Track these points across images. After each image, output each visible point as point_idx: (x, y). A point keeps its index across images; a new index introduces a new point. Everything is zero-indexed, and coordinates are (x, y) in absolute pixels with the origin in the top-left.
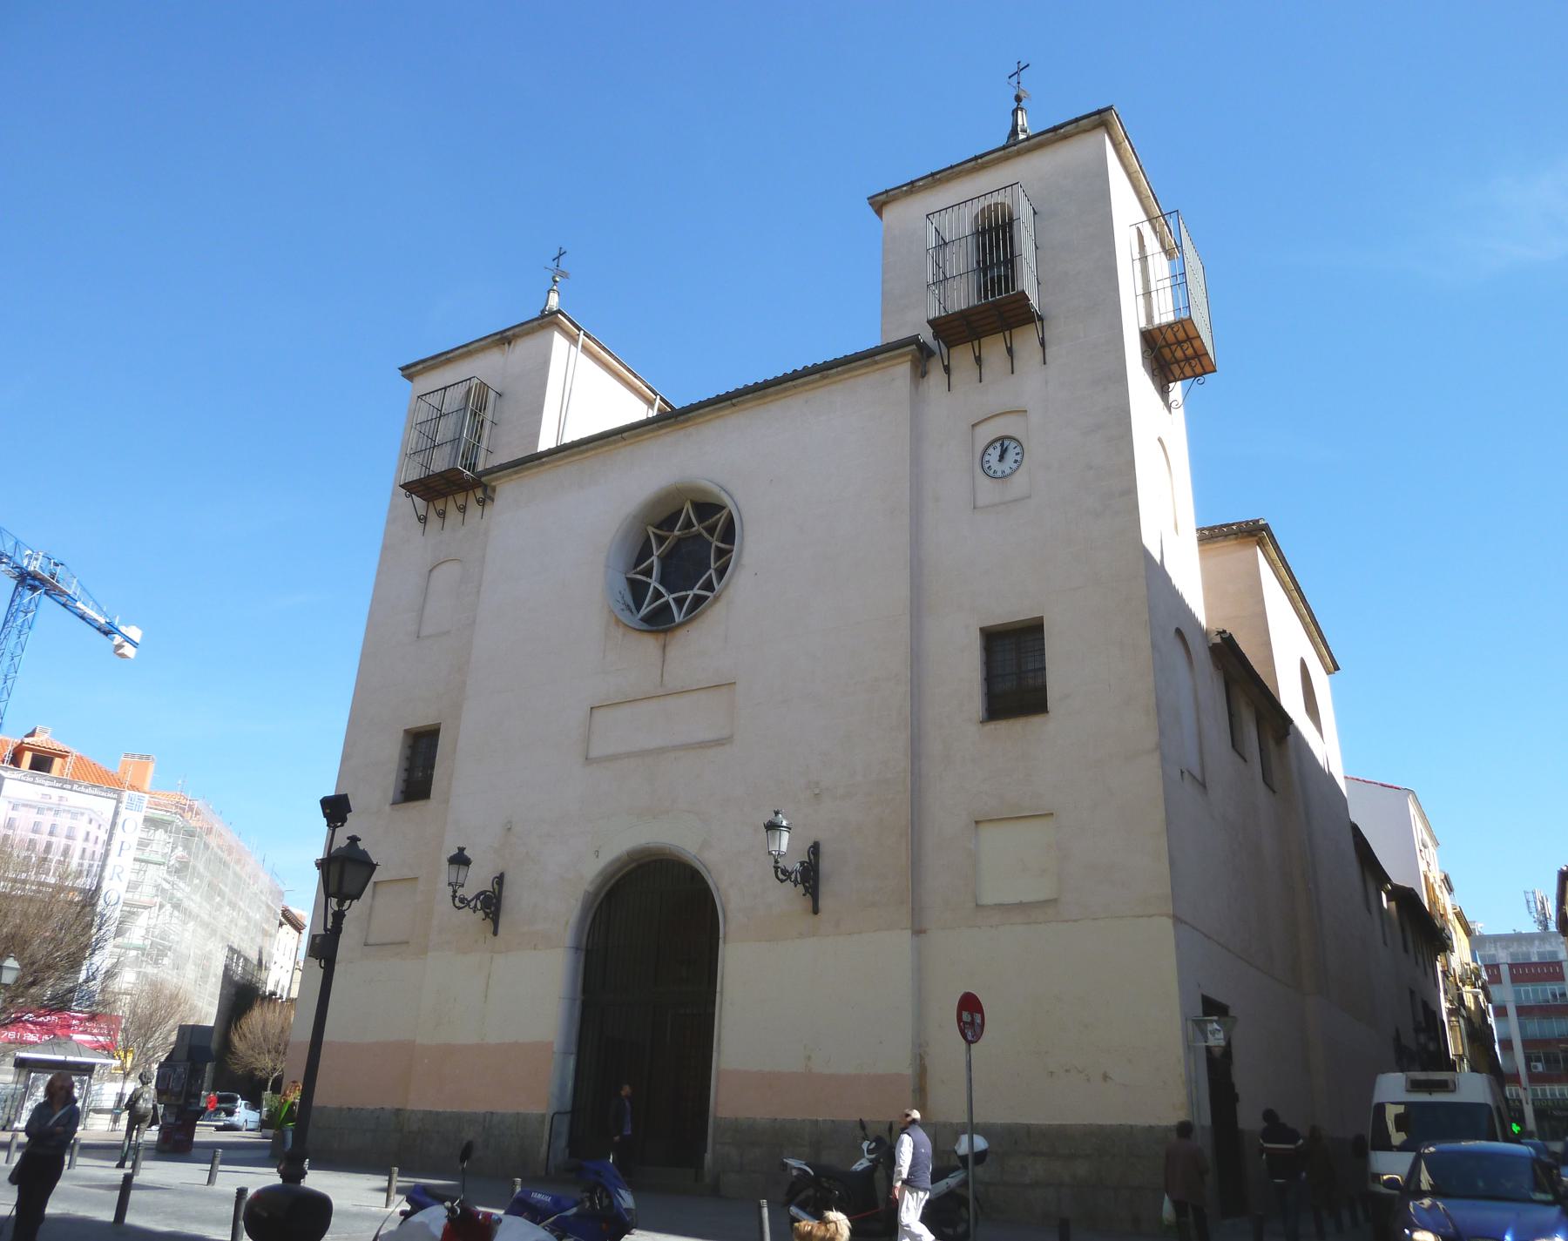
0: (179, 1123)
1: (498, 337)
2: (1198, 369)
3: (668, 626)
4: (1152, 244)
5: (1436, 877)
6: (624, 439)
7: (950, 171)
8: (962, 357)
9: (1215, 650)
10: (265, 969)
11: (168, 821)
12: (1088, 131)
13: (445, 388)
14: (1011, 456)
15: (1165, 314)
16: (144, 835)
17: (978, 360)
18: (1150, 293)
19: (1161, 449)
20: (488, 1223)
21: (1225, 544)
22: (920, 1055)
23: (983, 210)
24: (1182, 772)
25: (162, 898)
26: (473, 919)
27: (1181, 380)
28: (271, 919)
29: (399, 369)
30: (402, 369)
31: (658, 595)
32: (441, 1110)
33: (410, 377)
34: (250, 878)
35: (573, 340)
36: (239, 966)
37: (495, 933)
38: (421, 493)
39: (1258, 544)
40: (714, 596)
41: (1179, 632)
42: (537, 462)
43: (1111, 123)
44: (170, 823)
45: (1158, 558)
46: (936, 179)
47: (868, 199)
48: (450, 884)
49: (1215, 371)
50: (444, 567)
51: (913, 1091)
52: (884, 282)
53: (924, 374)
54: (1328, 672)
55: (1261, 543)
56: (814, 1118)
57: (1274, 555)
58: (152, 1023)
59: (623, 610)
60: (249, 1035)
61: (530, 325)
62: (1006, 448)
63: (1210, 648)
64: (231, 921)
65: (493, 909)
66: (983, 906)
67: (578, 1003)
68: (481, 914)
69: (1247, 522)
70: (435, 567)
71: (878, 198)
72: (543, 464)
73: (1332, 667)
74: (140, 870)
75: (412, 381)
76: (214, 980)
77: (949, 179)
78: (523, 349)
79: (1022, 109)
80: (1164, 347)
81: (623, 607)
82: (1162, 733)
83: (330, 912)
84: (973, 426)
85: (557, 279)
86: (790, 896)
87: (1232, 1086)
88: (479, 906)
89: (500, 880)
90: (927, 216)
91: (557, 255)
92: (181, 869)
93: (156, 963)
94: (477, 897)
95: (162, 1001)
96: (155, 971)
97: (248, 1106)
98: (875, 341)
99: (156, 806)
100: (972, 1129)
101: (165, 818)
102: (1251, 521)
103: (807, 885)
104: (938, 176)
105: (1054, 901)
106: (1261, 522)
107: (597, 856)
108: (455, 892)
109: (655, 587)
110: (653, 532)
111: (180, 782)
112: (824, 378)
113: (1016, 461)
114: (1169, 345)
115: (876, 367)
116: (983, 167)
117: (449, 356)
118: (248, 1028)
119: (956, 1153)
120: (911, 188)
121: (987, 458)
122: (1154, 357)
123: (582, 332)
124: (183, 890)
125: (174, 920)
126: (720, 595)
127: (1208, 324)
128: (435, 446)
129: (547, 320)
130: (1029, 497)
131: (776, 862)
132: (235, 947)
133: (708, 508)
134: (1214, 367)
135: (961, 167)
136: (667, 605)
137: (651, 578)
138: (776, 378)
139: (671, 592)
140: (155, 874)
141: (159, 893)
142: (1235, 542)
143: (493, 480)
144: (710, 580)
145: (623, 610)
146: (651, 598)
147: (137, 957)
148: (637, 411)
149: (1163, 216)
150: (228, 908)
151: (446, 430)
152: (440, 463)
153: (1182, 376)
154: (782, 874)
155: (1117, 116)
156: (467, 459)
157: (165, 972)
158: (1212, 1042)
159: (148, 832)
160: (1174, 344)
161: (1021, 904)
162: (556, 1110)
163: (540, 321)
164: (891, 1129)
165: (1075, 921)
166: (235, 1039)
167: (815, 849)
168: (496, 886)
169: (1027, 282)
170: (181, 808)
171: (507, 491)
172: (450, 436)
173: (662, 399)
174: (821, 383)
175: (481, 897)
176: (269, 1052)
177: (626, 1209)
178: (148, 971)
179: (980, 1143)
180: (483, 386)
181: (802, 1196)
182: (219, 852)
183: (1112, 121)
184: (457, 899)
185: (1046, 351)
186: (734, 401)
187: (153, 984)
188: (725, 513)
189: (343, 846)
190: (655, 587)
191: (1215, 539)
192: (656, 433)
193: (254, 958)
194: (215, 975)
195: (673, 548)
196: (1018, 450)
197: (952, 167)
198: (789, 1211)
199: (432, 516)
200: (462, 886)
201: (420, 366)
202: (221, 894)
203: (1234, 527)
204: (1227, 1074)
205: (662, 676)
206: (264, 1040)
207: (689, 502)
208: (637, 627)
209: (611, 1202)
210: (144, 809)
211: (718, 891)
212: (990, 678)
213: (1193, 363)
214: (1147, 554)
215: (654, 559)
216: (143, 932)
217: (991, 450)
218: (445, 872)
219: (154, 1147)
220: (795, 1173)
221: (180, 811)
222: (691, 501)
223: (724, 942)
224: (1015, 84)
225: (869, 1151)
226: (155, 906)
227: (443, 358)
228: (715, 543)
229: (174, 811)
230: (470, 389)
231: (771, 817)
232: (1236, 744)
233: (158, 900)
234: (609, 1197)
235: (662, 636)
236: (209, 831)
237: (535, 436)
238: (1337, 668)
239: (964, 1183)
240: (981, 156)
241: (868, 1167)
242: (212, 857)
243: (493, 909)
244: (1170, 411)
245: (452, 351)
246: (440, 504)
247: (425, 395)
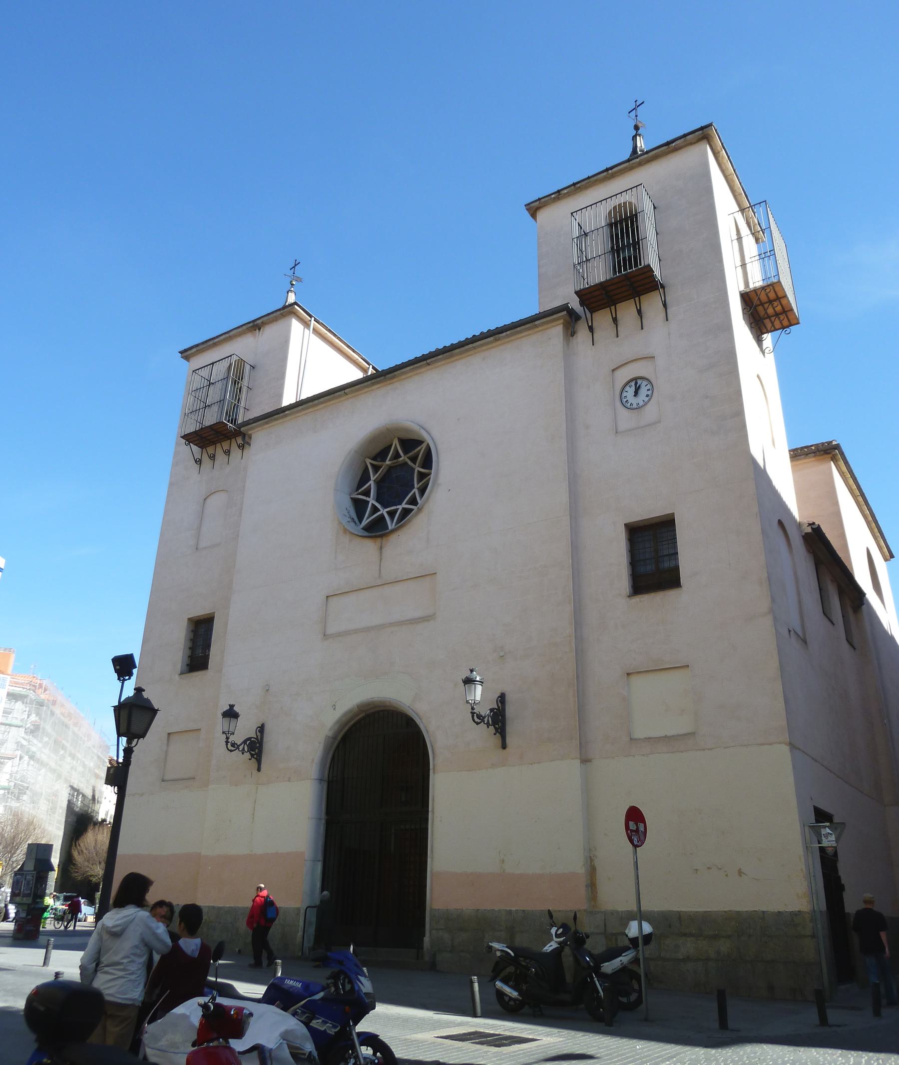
0: (30, 917)
2: (785, 323)
3: (383, 532)
6: (346, 394)
7: (588, 181)
8: (602, 319)
9: (807, 538)
10: (98, 803)
11: (24, 695)
12: (695, 143)
13: (213, 364)
14: (643, 391)
15: (756, 280)
16: (7, 706)
17: (615, 320)
20: (239, 1017)
21: (806, 461)
22: (590, 857)
23: (615, 208)
24: (789, 631)
25: (21, 751)
26: (242, 758)
27: (771, 331)
28: (101, 766)
29: (179, 352)
30: (181, 352)
32: (221, 905)
34: (85, 736)
35: (306, 325)
36: (78, 800)
37: (259, 770)
38: (198, 442)
39: (832, 460)
40: (418, 508)
41: (780, 523)
42: (282, 414)
43: (711, 136)
44: (26, 696)
45: (761, 464)
46: (577, 187)
48: (223, 733)
49: (798, 323)
50: (213, 497)
51: (586, 886)
52: (539, 267)
53: (573, 334)
54: (886, 560)
55: (834, 459)
56: (508, 909)
57: (844, 468)
58: (15, 844)
59: (349, 522)
60: (85, 851)
61: (275, 314)
62: (640, 386)
63: (803, 537)
64: (72, 768)
65: (257, 750)
66: (636, 739)
67: (323, 821)
68: (247, 755)
70: (207, 497)
72: (286, 416)
73: (889, 555)
74: (5, 732)
75: (189, 362)
76: (61, 811)
77: (586, 187)
78: (270, 332)
79: (640, 135)
81: (349, 520)
82: (773, 600)
83: (121, 748)
84: (613, 370)
85: (294, 283)
86: (484, 734)
88: (246, 749)
89: (261, 729)
90: (572, 214)
91: (296, 267)
92: (34, 730)
93: (18, 799)
94: (245, 742)
95: (21, 827)
96: (18, 805)
97: (86, 903)
98: (533, 310)
99: (16, 684)
100: (641, 916)
101: (22, 693)
102: (826, 443)
103: (497, 726)
104: (579, 185)
105: (692, 734)
106: (834, 443)
107: (335, 709)
108: (227, 738)
109: (372, 504)
110: (370, 463)
111: (32, 666)
112: (496, 340)
113: (647, 396)
114: (762, 304)
115: (536, 330)
116: (613, 176)
118: (84, 845)
119: (627, 936)
120: (559, 195)
121: (625, 394)
122: (751, 313)
123: (313, 319)
124: (36, 746)
125: (30, 768)
126: (422, 508)
127: (792, 287)
128: (206, 406)
129: (287, 311)
130: (659, 422)
131: (473, 709)
132: (75, 786)
133: (411, 443)
134: (798, 320)
135: (595, 178)
136: (382, 517)
137: (369, 497)
138: (460, 342)
139: (385, 507)
140: (17, 734)
141: (19, 748)
142: (814, 459)
144: (414, 497)
145: (349, 522)
146: (369, 515)
147: (4, 794)
148: (356, 375)
149: (751, 206)
150: (69, 758)
151: (214, 394)
152: (210, 419)
153: (773, 328)
154: (477, 718)
155: (716, 131)
156: (230, 416)
157: (25, 806)
158: (825, 843)
159: (10, 703)
160: (766, 303)
161: (666, 736)
162: (308, 905)
164: (575, 918)
165: (711, 749)
166: (75, 854)
167: (502, 698)
168: (259, 734)
169: (651, 257)
170: (33, 686)
171: (260, 437)
172: (217, 399)
173: (373, 368)
174: (494, 344)
175: (248, 742)
176: (100, 863)
177: (364, 993)
178: (12, 805)
179: (647, 928)
180: (241, 362)
181: (502, 975)
182: (62, 718)
183: (713, 135)
184: (229, 744)
185: (668, 311)
186: (428, 361)
187: (15, 815)
188: (424, 446)
190: (372, 504)
191: (798, 457)
192: (370, 389)
193: (89, 794)
194: (61, 807)
195: (385, 475)
196: (649, 387)
197: (589, 178)
198: (495, 985)
199: (205, 458)
200: (233, 734)
201: (194, 350)
202: (64, 748)
203: (813, 448)
204: (835, 869)
205: (380, 570)
206: (96, 855)
208: (360, 534)
209: (353, 988)
210: (7, 687)
211: (428, 733)
212: (634, 563)
214: (754, 462)
215: (371, 483)
216: (8, 777)
217: (627, 388)
218: (220, 724)
219: (11, 935)
220: (498, 954)
221: (34, 688)
222: (398, 438)
223: (434, 773)
224: (634, 117)
225: (557, 936)
226: (16, 757)
227: (211, 343)
228: (418, 469)
229: (28, 688)
230: (231, 365)
231: (468, 674)
232: (826, 613)
233: (19, 753)
234: (350, 982)
235: (379, 540)
236: (54, 703)
237: (280, 396)
238: (892, 556)
239: (636, 961)
241: (557, 947)
242: (57, 721)
243: (257, 750)
244: (764, 355)
245: (217, 337)
246: (211, 450)
247: (198, 369)
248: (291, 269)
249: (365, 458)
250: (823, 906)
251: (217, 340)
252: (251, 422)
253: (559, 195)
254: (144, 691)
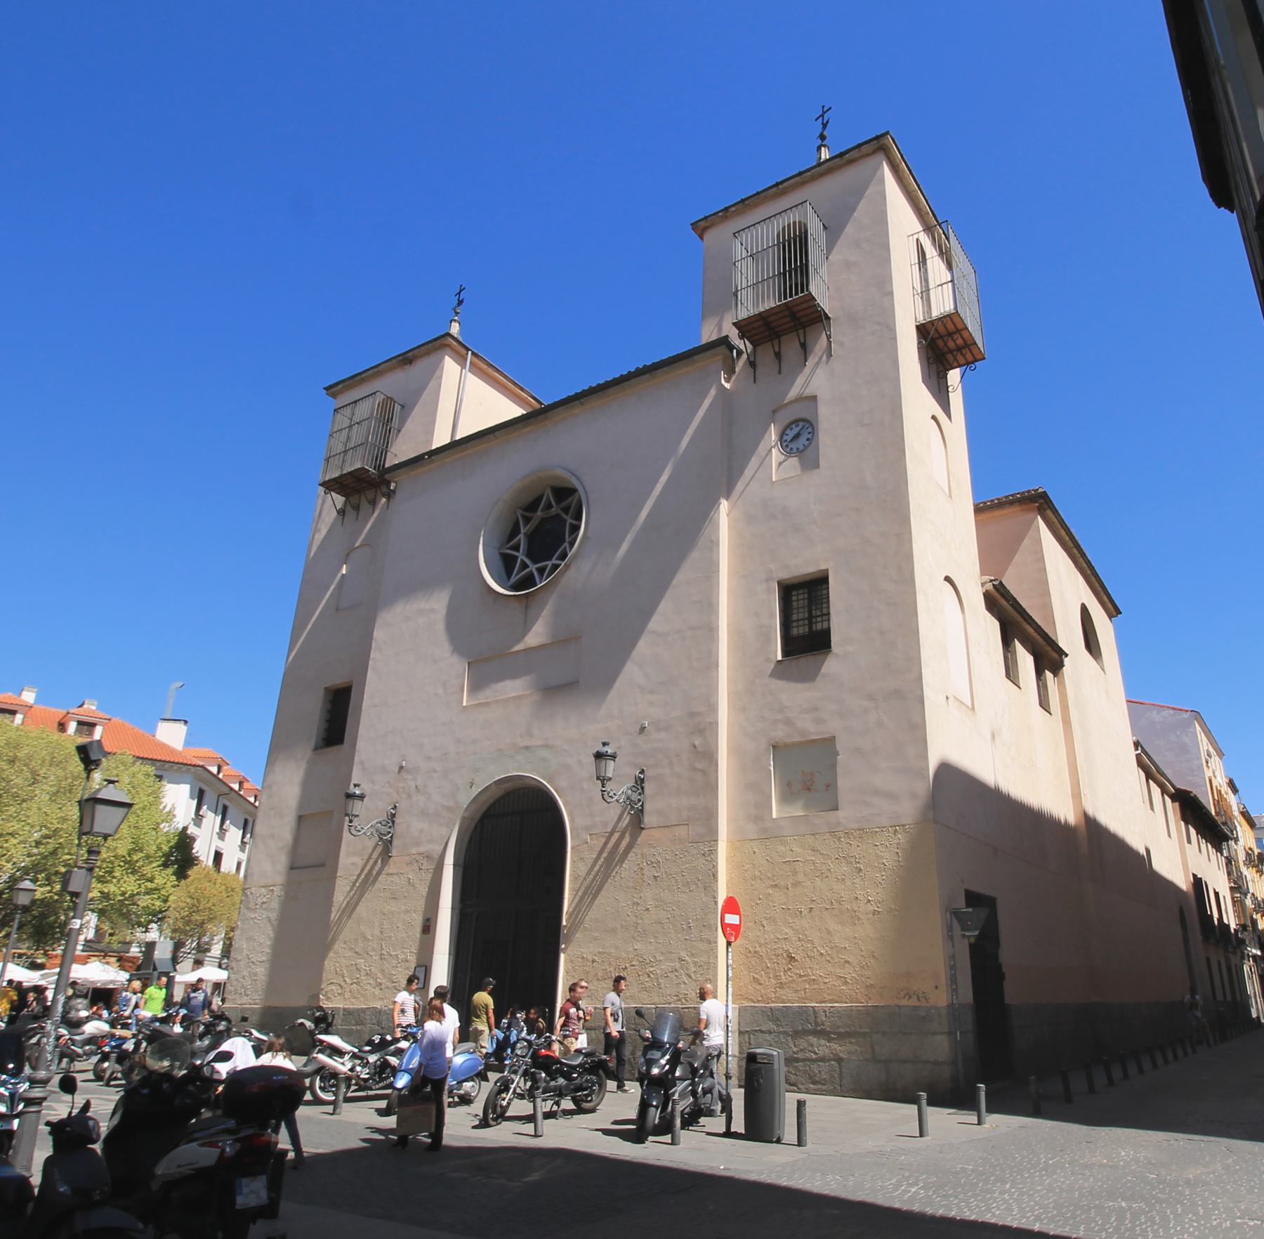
1: (401, 358)
4: (931, 251)
5: (1221, 781)
17: (778, 355)
18: (929, 290)
19: (936, 425)
29: (324, 388)
30: (327, 389)
31: (525, 566)
33: (334, 396)
47: (691, 225)
49: (984, 359)
54: (1110, 616)
55: (1041, 511)
69: (1029, 491)
73: (1113, 610)
78: (420, 366)
79: (825, 146)
80: (937, 339)
87: (999, 966)
90: (734, 234)
104: (747, 202)
106: (1040, 490)
109: (521, 560)
113: (808, 439)
114: (941, 337)
117: (363, 376)
129: (440, 343)
137: (519, 552)
139: (535, 562)
142: (1019, 508)
146: (519, 568)
148: (514, 411)
151: (357, 435)
152: (354, 464)
155: (893, 141)
171: (402, 484)
190: (521, 560)
201: (340, 386)
207: (549, 489)
213: (964, 351)
228: (570, 521)
240: (782, 182)
246: (354, 500)
250: (966, 994)
254: (1067, 655)
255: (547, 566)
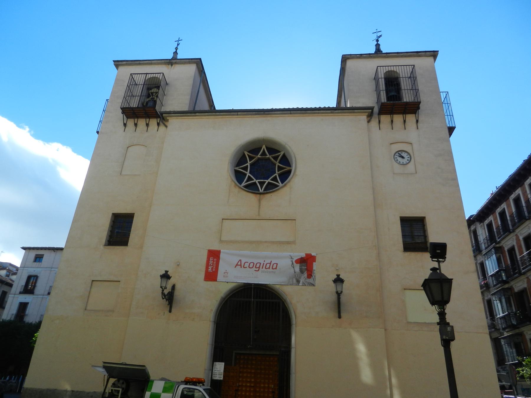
1: (168, 61)
8: (386, 119)
12: (428, 57)
29: (113, 61)
30: (114, 61)
66: (411, 323)
71: (346, 56)
90: (131, 74)
104: (372, 55)
112: (331, 113)
113: (408, 160)
137: (247, 171)
143: (168, 117)
163: (190, 61)
171: (174, 122)
189: (314, 263)
201: (124, 63)
227: (138, 62)
247: (134, 74)
248: (175, 41)
249: (245, 151)
251: (143, 62)
252: (172, 113)
253: (361, 56)
255: (271, 180)
